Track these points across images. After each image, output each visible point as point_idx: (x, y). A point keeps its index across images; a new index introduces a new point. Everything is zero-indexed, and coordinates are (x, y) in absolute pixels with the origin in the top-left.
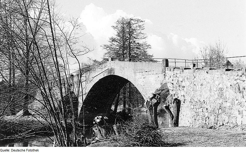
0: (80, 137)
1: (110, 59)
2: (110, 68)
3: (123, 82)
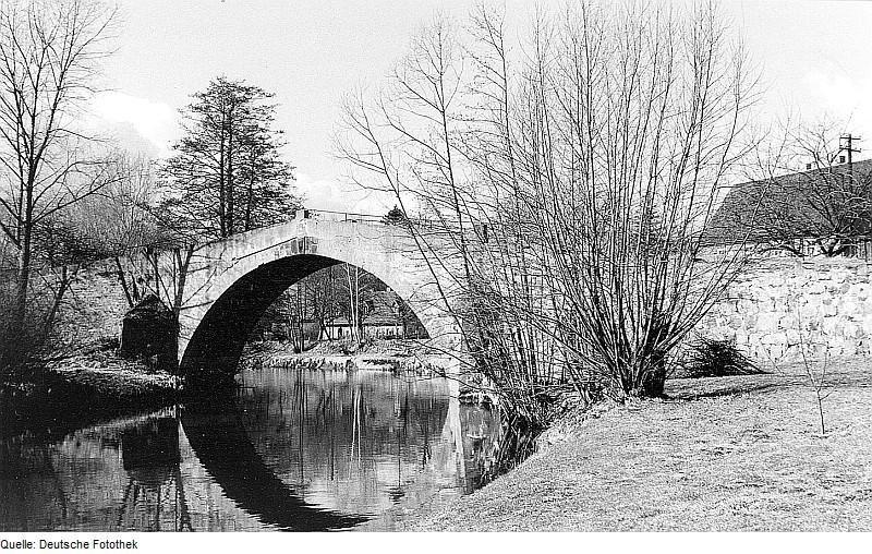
2: (300, 236)
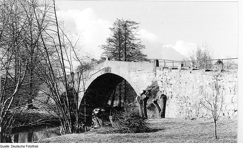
0: (82, 125)
1: (107, 59)
3: (117, 79)
